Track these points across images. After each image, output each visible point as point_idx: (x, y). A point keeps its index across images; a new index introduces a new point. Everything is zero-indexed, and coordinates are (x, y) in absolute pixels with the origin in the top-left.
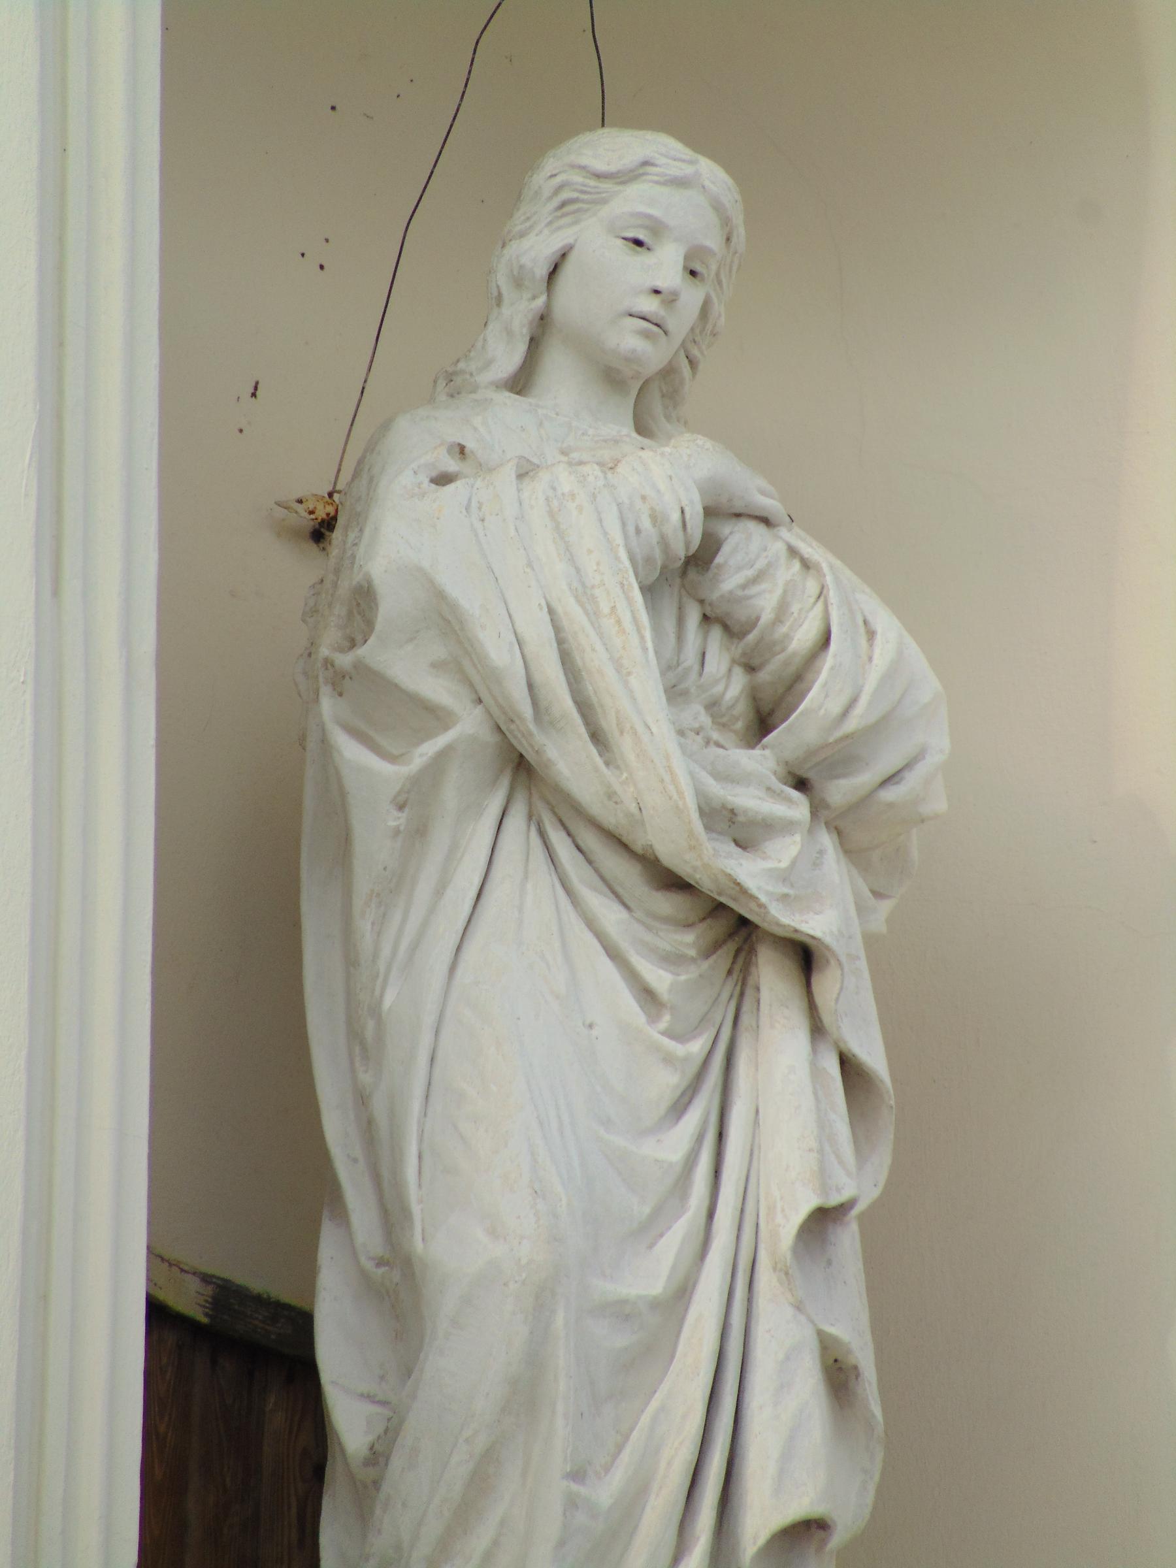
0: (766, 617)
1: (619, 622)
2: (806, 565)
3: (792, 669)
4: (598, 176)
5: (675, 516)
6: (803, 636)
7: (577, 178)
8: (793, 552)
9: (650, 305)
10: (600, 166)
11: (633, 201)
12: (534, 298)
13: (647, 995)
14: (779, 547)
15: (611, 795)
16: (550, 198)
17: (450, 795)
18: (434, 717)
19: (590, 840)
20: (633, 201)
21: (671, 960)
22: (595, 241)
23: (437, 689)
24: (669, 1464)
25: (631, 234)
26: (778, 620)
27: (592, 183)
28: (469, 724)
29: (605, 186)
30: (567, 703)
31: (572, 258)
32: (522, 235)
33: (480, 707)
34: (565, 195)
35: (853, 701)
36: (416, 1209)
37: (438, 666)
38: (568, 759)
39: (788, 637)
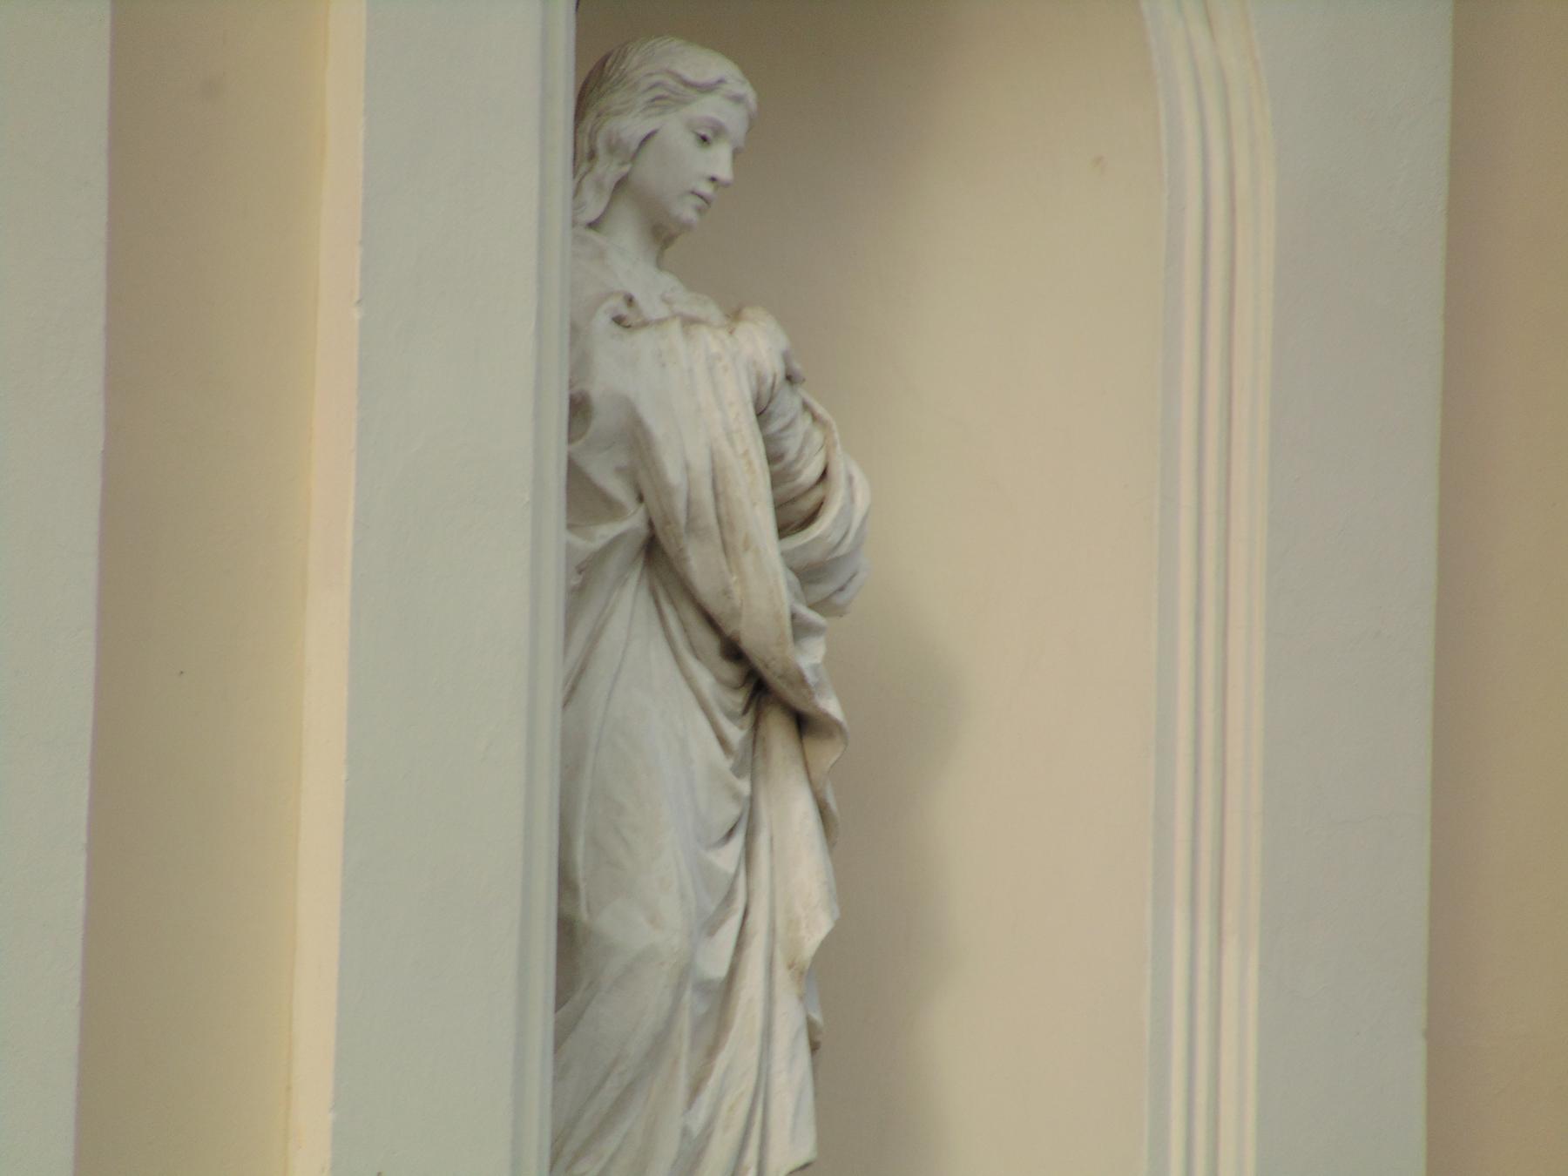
0: (791, 456)
1: (750, 463)
2: (815, 418)
3: (793, 495)
4: (687, 84)
5: (770, 380)
6: (811, 472)
7: (671, 82)
8: (806, 406)
9: (706, 189)
10: (690, 76)
11: (709, 108)
12: (623, 164)
13: (723, 742)
14: (797, 403)
15: (727, 592)
16: (644, 92)
17: (613, 565)
18: (611, 508)
19: (692, 617)
20: (709, 108)
21: (731, 716)
22: (674, 128)
23: (617, 488)
24: (731, 1108)
25: (703, 132)
26: (797, 460)
27: (681, 87)
28: (633, 522)
29: (691, 92)
30: (712, 521)
31: (657, 137)
32: (618, 113)
33: (641, 509)
34: (658, 92)
35: (846, 534)
36: (582, 886)
37: (619, 471)
38: (700, 563)
39: (799, 472)
